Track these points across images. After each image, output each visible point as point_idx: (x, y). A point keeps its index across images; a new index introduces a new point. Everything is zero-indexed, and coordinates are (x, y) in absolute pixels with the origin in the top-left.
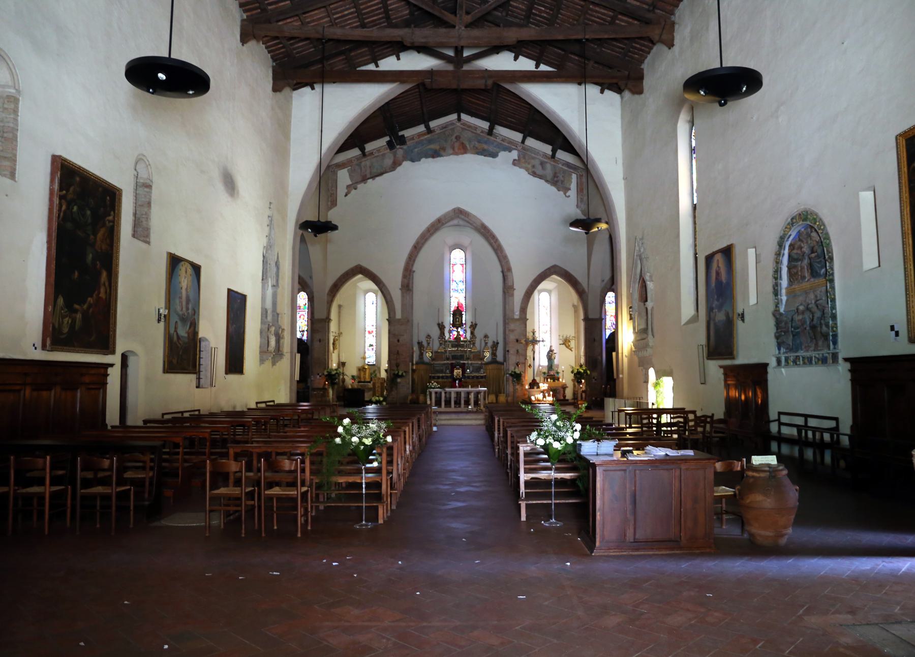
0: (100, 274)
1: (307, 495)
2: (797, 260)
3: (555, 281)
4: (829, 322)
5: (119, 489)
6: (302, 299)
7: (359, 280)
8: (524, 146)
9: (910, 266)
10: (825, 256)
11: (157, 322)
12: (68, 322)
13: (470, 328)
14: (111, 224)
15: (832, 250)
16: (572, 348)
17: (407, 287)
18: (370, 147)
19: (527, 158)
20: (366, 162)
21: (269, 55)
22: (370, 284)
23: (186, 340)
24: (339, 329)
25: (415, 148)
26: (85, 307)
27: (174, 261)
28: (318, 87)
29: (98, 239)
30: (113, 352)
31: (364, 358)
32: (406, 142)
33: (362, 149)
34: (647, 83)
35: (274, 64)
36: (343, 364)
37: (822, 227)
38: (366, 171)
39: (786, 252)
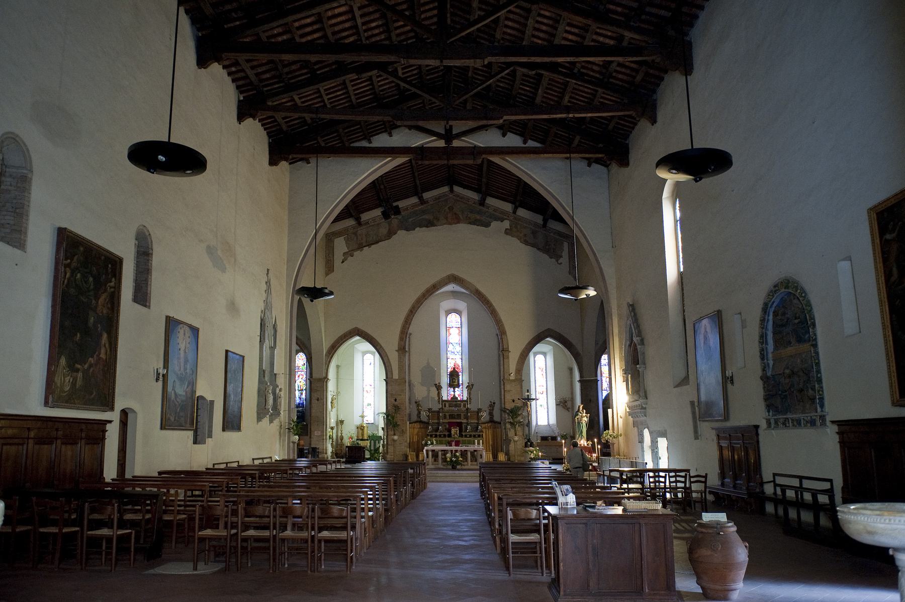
0: (101, 335)
1: (131, 537)
2: (783, 326)
3: (549, 343)
4: (815, 386)
5: (120, 532)
6: (301, 360)
7: (357, 342)
8: (515, 216)
9: (889, 332)
10: (807, 322)
11: (155, 381)
12: (69, 381)
13: (466, 388)
14: (112, 290)
15: (814, 316)
16: (569, 408)
17: (403, 349)
18: (365, 217)
19: (519, 227)
20: (362, 231)
21: (265, 132)
22: (368, 346)
23: (184, 398)
24: (337, 388)
25: (410, 218)
26: (86, 366)
27: (171, 324)
28: (313, 161)
29: (99, 302)
30: (112, 409)
31: (363, 417)
32: (400, 213)
33: (358, 220)
34: (633, 157)
35: (271, 141)
36: (342, 422)
37: (803, 295)
38: (362, 240)
39: (771, 317)
